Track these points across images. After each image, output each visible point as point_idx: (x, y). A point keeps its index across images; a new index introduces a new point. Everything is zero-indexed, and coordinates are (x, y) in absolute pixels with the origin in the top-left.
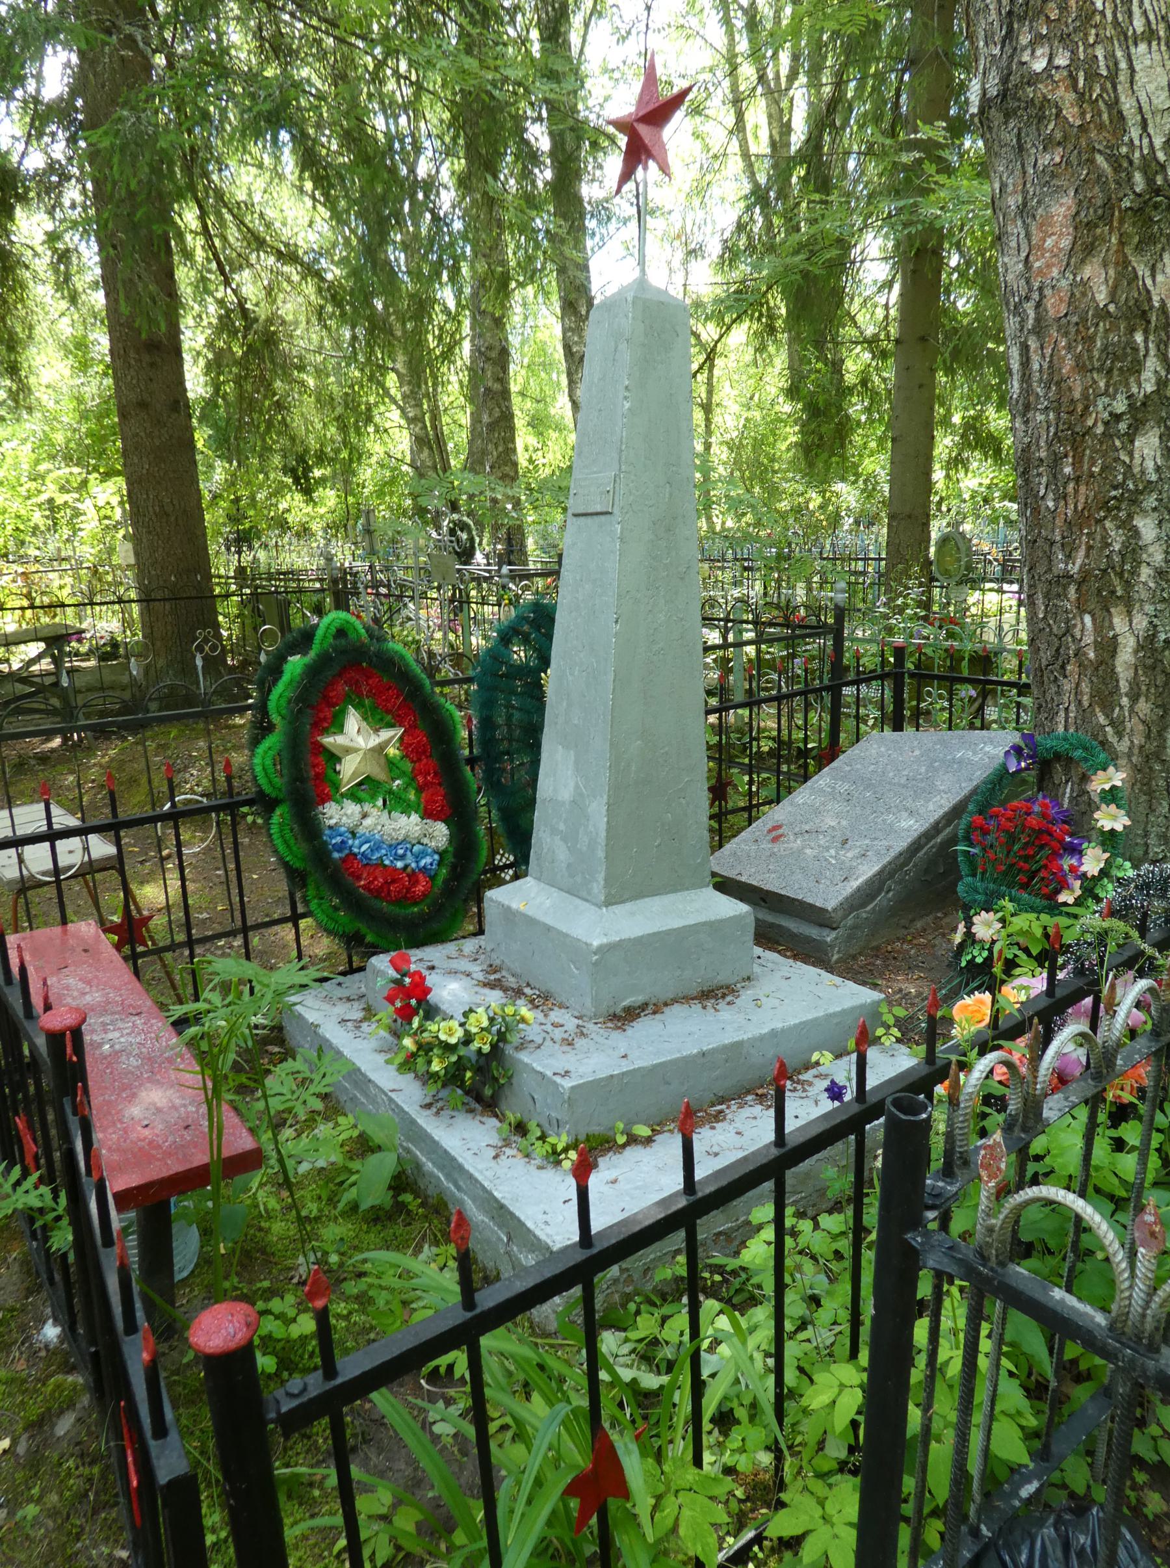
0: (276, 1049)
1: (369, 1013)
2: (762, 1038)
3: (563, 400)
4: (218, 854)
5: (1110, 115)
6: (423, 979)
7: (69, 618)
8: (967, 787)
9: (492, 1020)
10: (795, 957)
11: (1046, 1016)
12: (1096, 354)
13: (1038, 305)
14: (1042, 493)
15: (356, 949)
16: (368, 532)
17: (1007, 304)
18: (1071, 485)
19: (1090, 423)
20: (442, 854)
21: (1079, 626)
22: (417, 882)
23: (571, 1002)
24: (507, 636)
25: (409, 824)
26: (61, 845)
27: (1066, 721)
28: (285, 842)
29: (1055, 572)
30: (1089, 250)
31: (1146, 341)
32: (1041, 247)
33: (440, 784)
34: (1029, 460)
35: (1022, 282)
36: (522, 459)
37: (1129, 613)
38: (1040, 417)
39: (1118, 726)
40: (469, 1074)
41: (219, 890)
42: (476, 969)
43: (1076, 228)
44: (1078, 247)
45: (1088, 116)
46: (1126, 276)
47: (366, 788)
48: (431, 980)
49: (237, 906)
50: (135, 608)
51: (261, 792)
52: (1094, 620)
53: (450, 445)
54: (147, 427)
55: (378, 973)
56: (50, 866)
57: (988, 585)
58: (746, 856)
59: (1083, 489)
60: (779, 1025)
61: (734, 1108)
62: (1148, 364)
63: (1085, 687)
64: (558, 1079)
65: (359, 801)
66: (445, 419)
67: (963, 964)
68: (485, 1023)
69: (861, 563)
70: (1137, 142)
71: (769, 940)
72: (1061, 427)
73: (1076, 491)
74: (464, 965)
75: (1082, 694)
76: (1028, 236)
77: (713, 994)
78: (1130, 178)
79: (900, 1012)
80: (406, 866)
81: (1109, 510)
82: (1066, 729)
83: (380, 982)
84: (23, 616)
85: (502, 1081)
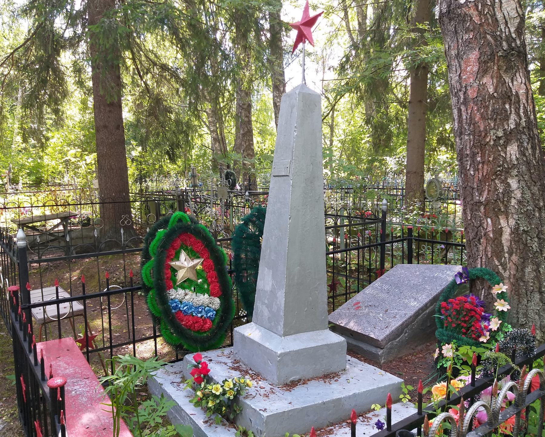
0: (144, 394)
1: (184, 379)
2: (349, 397)
3: (273, 124)
4: (125, 308)
5: (492, 20)
6: (207, 365)
7: (71, 209)
8: (439, 289)
9: (234, 385)
10: (365, 361)
11: (471, 394)
12: (489, 112)
13: (465, 93)
14: (468, 168)
15: (179, 352)
16: (194, 176)
17: (452, 92)
18: (481, 165)
19: (488, 140)
20: (217, 311)
22: (206, 323)
23: (268, 378)
24: (247, 221)
25: (204, 298)
26: (61, 305)
27: (481, 263)
28: (153, 305)
29: (475, 200)
30: (485, 72)
31: (510, 107)
33: (217, 282)
34: (462, 154)
35: (458, 84)
36: (256, 147)
37: (507, 218)
38: (467, 138)
39: (504, 265)
40: (224, 408)
41: (125, 323)
42: (229, 361)
43: (479, 63)
44: (481, 71)
45: (483, 20)
46: (501, 82)
47: (187, 284)
48: (210, 366)
49: (131, 331)
50: (98, 206)
51: (144, 285)
52: (492, 221)
53: (227, 141)
54: (107, 135)
55: (188, 362)
56: (56, 313)
57: (449, 201)
58: (345, 317)
59: (485, 167)
60: (357, 392)
61: (337, 428)
62: (511, 117)
63: (489, 249)
64: (261, 412)
65: (183, 288)
66: (225, 131)
67: (438, 367)
68: (232, 386)
69: (395, 190)
70: (503, 30)
71: (354, 352)
72: (476, 142)
73: (483, 168)
74: (224, 359)
75: (488, 251)
76: (460, 66)
77: (329, 376)
78: (501, 44)
79: (410, 388)
80: (202, 316)
81: (497, 176)
82: (481, 266)
83: (189, 366)
84: (53, 208)
85: (238, 412)
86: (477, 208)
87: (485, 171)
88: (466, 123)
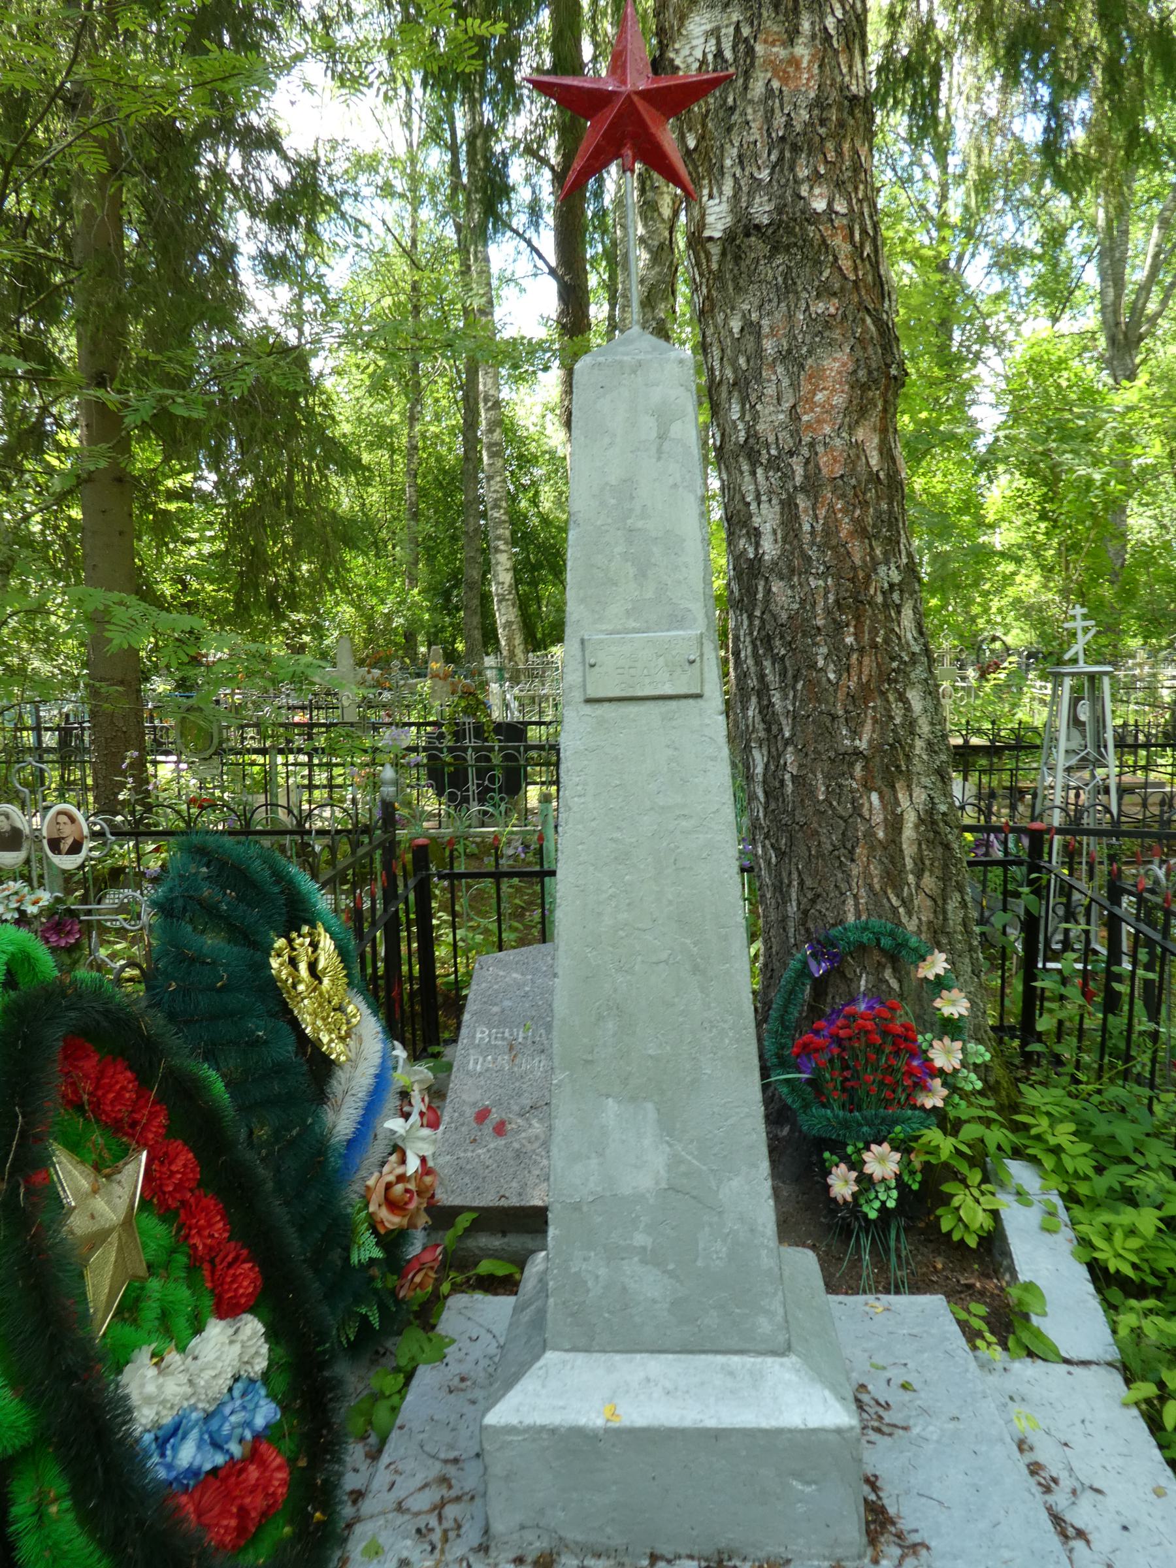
18: (855, 656)
21: (867, 805)
32: (810, 400)
37: (909, 787)
52: (881, 798)
59: (866, 660)
73: (860, 663)
82: (858, 917)
86: (845, 768)
87: (866, 672)
88: (813, 543)
